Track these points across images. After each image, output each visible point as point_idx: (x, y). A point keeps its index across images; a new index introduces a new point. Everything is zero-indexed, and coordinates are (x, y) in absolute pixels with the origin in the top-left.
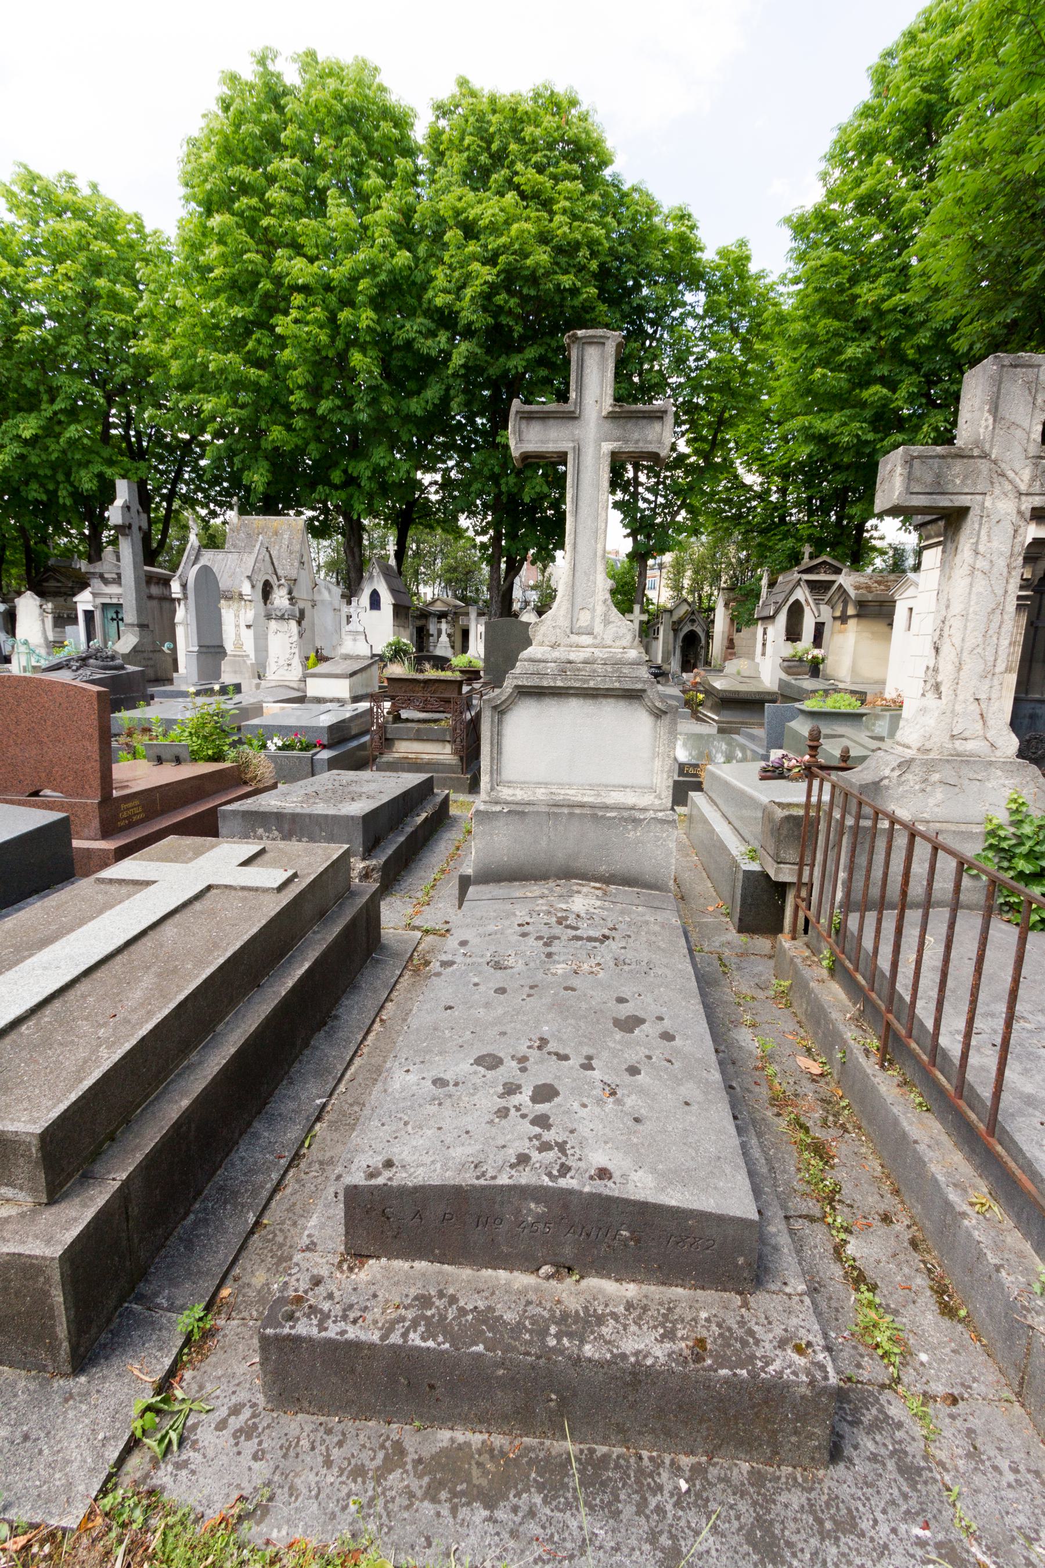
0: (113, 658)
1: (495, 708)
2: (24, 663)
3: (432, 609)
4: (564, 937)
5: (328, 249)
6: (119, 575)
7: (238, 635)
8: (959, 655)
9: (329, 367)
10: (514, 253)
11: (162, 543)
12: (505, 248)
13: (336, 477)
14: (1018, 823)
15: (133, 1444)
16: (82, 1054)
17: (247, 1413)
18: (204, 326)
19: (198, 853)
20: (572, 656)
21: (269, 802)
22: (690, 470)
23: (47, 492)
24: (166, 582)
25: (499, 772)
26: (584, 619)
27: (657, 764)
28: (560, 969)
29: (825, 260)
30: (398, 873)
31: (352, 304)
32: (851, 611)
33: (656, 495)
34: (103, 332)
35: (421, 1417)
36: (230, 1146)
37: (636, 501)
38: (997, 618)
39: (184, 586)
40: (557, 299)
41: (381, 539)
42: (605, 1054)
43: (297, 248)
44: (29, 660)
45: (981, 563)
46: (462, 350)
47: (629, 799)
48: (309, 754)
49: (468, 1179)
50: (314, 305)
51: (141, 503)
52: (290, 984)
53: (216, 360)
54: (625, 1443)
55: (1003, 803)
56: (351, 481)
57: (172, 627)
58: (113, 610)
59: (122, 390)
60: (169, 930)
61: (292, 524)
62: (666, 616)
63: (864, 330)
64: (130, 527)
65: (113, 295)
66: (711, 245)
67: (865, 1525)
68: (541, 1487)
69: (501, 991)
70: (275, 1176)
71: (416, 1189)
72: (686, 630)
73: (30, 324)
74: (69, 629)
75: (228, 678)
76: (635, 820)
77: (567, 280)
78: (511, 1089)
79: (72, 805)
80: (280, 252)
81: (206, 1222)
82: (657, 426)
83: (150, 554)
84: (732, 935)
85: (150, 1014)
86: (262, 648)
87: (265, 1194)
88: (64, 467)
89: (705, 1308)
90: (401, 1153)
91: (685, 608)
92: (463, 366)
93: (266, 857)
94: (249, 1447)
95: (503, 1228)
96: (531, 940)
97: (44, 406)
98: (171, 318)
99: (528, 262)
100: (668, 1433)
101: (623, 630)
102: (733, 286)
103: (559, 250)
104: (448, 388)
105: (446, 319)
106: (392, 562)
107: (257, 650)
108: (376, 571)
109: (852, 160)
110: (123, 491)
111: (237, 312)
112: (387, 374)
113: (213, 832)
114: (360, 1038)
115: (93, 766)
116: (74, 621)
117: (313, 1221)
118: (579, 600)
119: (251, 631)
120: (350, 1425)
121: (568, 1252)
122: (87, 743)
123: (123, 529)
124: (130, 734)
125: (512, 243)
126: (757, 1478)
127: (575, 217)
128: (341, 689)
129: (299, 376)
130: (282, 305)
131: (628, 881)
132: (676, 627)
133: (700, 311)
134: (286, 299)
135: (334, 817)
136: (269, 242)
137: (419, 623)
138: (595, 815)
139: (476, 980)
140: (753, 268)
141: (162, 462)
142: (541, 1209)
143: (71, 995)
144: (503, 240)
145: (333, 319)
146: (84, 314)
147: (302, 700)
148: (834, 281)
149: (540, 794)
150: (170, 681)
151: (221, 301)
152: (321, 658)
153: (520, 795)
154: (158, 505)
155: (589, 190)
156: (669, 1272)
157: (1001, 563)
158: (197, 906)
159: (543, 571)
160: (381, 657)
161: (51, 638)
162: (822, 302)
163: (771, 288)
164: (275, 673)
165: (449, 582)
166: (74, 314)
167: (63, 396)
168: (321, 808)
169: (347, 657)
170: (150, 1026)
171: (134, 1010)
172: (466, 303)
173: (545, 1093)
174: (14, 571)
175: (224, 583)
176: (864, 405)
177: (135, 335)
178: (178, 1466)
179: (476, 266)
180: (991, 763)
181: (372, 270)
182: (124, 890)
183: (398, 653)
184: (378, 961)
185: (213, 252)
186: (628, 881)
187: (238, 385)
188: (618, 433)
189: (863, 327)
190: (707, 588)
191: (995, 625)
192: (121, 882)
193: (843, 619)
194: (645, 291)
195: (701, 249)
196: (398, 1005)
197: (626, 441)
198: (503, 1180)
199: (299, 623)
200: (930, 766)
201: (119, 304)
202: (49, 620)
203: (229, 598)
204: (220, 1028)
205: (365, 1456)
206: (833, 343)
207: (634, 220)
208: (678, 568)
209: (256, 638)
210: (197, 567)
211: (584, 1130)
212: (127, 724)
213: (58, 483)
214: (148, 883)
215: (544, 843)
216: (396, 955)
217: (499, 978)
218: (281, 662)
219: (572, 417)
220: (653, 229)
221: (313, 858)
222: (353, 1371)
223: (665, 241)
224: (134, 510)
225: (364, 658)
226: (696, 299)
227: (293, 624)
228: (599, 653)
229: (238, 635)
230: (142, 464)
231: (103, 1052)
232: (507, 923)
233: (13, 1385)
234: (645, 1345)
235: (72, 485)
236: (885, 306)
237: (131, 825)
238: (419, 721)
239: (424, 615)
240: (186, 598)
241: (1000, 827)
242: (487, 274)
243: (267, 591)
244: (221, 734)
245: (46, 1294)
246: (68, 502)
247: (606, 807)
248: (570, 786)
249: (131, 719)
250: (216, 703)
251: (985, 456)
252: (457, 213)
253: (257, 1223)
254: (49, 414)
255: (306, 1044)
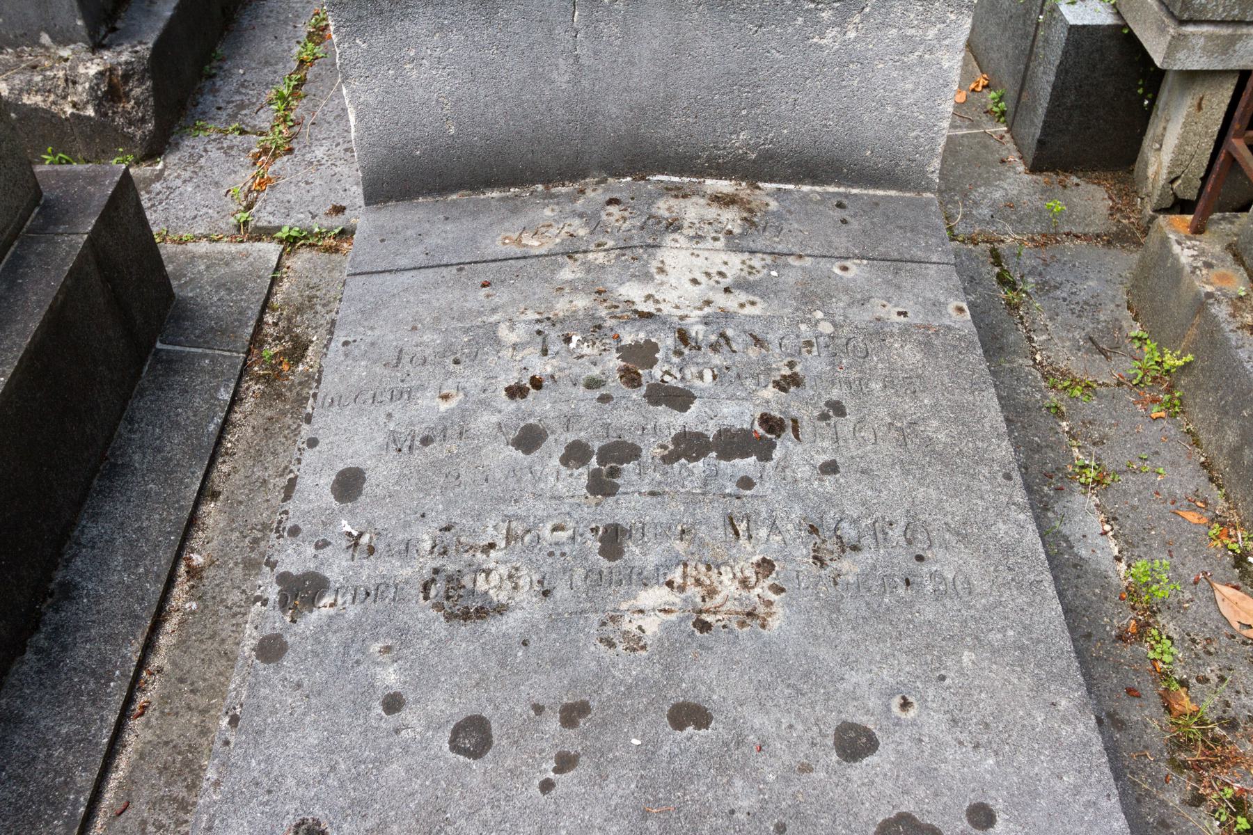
4: (651, 450)
28: (651, 609)
84: (1018, 181)
114: (133, 652)
139: (390, 677)
196: (233, 504)
215: (562, 78)
216: (219, 333)
232: (474, 380)
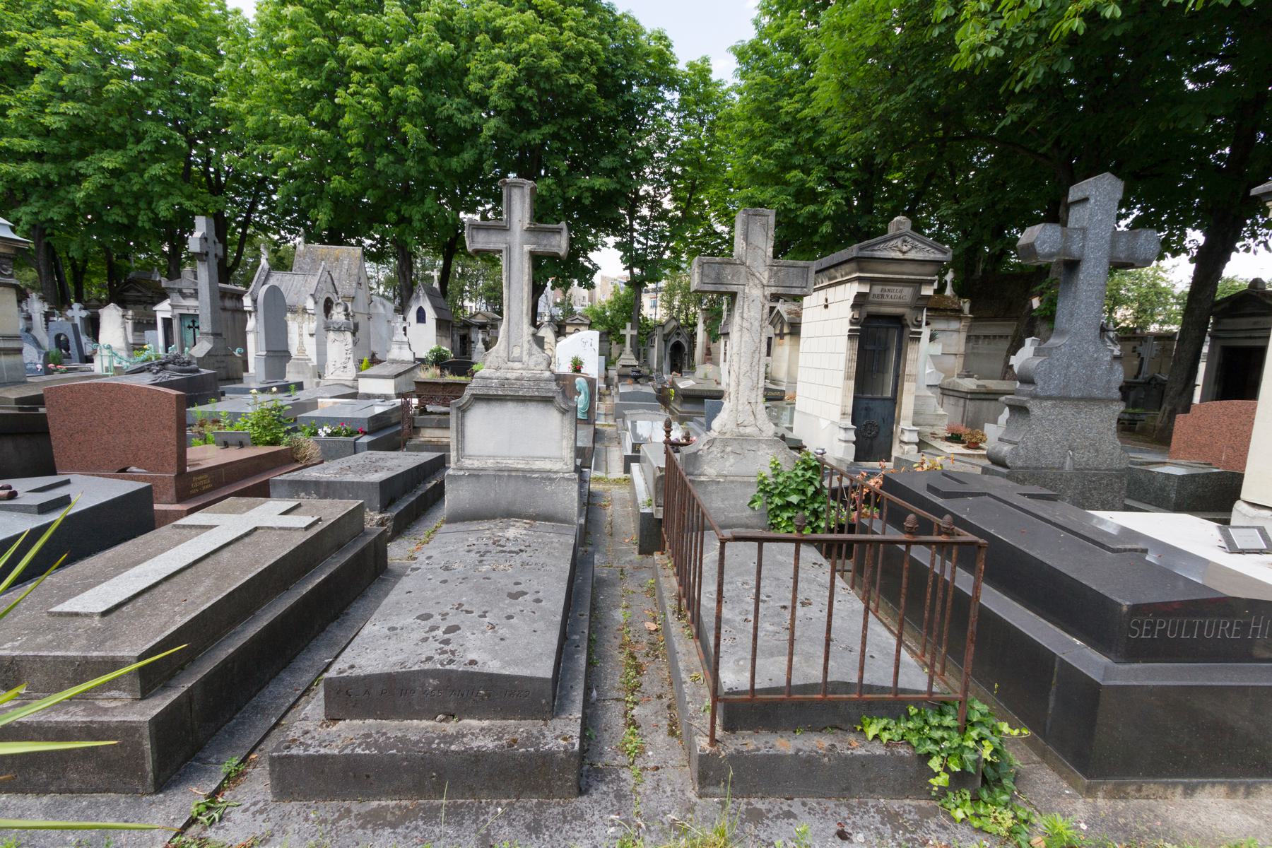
0: (189, 363)
1: (459, 408)
2: (106, 364)
3: (473, 320)
5: (382, 39)
6: (196, 290)
7: (301, 343)
8: (738, 377)
9: (381, 133)
10: (533, 56)
11: (238, 259)
12: (523, 53)
13: (392, 216)
14: (776, 476)
15: (192, 821)
16: (163, 619)
17: (261, 804)
18: (276, 90)
19: (250, 508)
20: (508, 376)
21: (312, 474)
22: (671, 221)
23: (128, 216)
24: (239, 296)
25: (463, 449)
26: (516, 352)
27: (565, 443)
28: (484, 568)
29: (758, 80)
30: (410, 523)
31: (402, 83)
32: (786, 330)
33: (647, 239)
34: (187, 87)
35: (362, 795)
36: (262, 685)
37: (632, 242)
38: (757, 355)
39: (255, 301)
40: (566, 91)
41: (430, 265)
42: (496, 610)
43: (357, 36)
44: (111, 362)
45: (745, 324)
46: (491, 125)
47: (547, 465)
48: (352, 439)
49: (397, 669)
50: (370, 81)
51: (217, 234)
52: (310, 587)
53: (285, 120)
54: (473, 796)
55: (768, 464)
56: (403, 220)
57: (244, 334)
58: (191, 321)
59: (203, 135)
60: (225, 554)
61: (348, 255)
62: (659, 330)
63: (788, 130)
64: (207, 254)
65: (193, 59)
66: (683, 58)
67: (587, 817)
68: (423, 818)
69: (445, 581)
70: (292, 700)
71: (366, 677)
72: (673, 341)
73: (119, 77)
74: (148, 333)
75: (291, 377)
76: (550, 479)
77: (573, 79)
78: (433, 629)
79: (152, 479)
80: (342, 39)
81: (243, 724)
82: (558, 237)
83: (225, 272)
85: (209, 599)
86: (322, 353)
87: (284, 709)
88: (145, 197)
89: (520, 727)
90: (357, 662)
91: (674, 323)
92: (493, 137)
93: (301, 510)
94: (260, 818)
95: (416, 695)
96: (472, 554)
97: (130, 146)
98: (247, 83)
99: (543, 63)
100: (496, 788)
101: (541, 360)
102: (698, 88)
103: (567, 57)
104: (481, 153)
105: (481, 101)
106: (436, 285)
107: (318, 354)
108: (422, 292)
109: (776, 12)
110: (201, 226)
111: (304, 83)
112: (431, 137)
113: (267, 495)
115: (172, 449)
116: (153, 326)
117: (309, 707)
118: (513, 341)
119: (314, 340)
120: (321, 804)
121: (452, 706)
122: (167, 433)
123: (201, 256)
124: (202, 425)
125: (530, 48)
126: (540, 805)
127: (579, 34)
128: (388, 387)
129: (354, 136)
130: (345, 79)
131: (548, 518)
132: (666, 338)
133: (676, 106)
134: (348, 74)
135: (358, 483)
136: (334, 31)
137: (462, 332)
138: (525, 476)
140: (714, 77)
141: (238, 194)
142: (436, 682)
143: (156, 591)
144: (524, 46)
145: (384, 92)
146: (169, 72)
147: (354, 396)
148: (765, 95)
149: (490, 463)
150: (240, 380)
151: (293, 73)
152: (374, 361)
153: (477, 464)
154: (235, 229)
155: (591, 15)
156: (506, 712)
157: (757, 324)
158: (247, 540)
159: (565, 293)
160: (422, 361)
161: (131, 341)
162: (758, 109)
163: (725, 93)
164: (332, 375)
165: (488, 299)
166: (160, 74)
167: (148, 139)
168: (350, 477)
169: (394, 362)
170: (209, 605)
171: (198, 597)
172: (494, 90)
173: (453, 629)
174: (95, 280)
175: (290, 299)
176: (787, 183)
177: (215, 93)
178: (218, 828)
179: (500, 64)
180: (759, 441)
181: (418, 57)
182: (194, 532)
183: (439, 360)
184: (383, 580)
185: (287, 34)
186: (548, 518)
187: (305, 141)
188: (534, 240)
189: (786, 128)
190: (692, 309)
191: (756, 360)
192: (191, 527)
193: (781, 335)
194: (635, 89)
195: (675, 63)
197: (539, 245)
198: (416, 668)
199: (354, 334)
200: (726, 442)
201: (199, 68)
202: (130, 325)
203: (294, 312)
204: (259, 612)
205: (328, 816)
206: (766, 138)
207: (624, 39)
208: (671, 291)
209: (318, 345)
210: (266, 287)
211: (469, 645)
212: (199, 416)
213: (140, 209)
214: (211, 527)
217: (445, 575)
218: (338, 365)
219: (505, 229)
220: (638, 46)
221: (334, 510)
222: (323, 772)
223: (648, 54)
224: (210, 241)
225: (408, 362)
226: (673, 96)
227: (349, 335)
228: (525, 373)
229: (301, 343)
230: (221, 198)
231: (178, 618)
233: (117, 801)
234: (489, 744)
235: (153, 211)
236: (798, 116)
237: (201, 493)
238: (440, 413)
239: (467, 325)
240: (256, 310)
241: (765, 478)
242: (508, 71)
243: (328, 306)
244: (279, 424)
245: (140, 744)
246: (147, 226)
247: (533, 471)
248: (510, 458)
249: (203, 412)
250: (284, 400)
251: (743, 264)
252: (488, 21)
253: (277, 724)
254: (133, 153)
255: (323, 629)
